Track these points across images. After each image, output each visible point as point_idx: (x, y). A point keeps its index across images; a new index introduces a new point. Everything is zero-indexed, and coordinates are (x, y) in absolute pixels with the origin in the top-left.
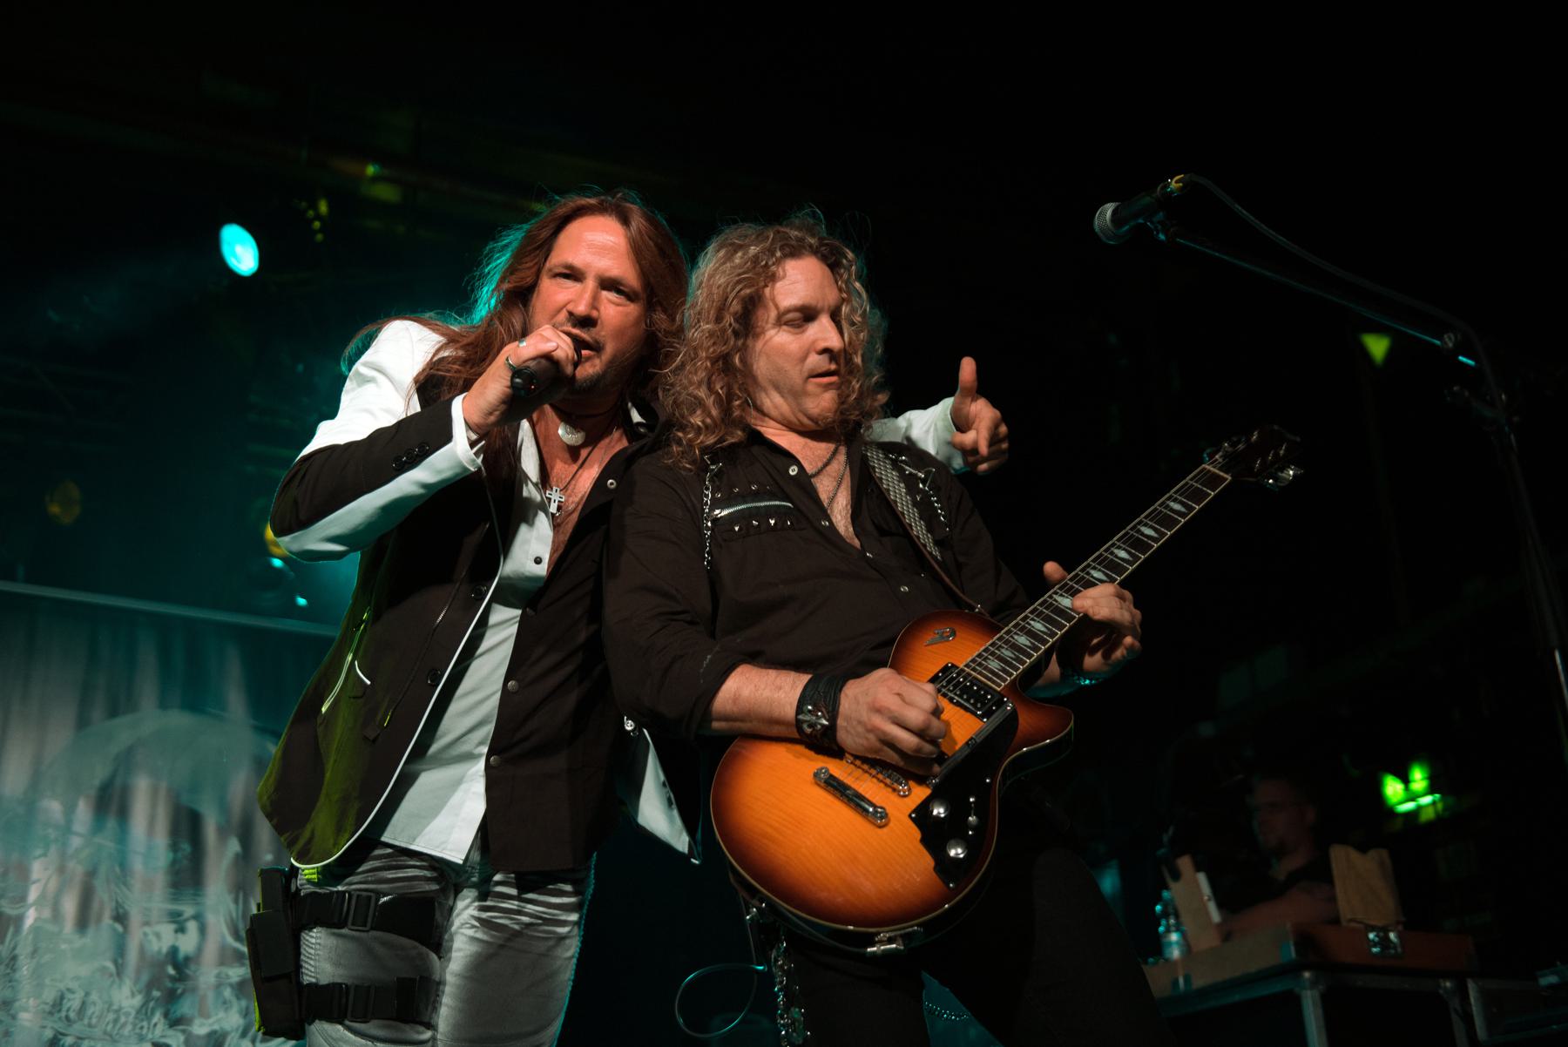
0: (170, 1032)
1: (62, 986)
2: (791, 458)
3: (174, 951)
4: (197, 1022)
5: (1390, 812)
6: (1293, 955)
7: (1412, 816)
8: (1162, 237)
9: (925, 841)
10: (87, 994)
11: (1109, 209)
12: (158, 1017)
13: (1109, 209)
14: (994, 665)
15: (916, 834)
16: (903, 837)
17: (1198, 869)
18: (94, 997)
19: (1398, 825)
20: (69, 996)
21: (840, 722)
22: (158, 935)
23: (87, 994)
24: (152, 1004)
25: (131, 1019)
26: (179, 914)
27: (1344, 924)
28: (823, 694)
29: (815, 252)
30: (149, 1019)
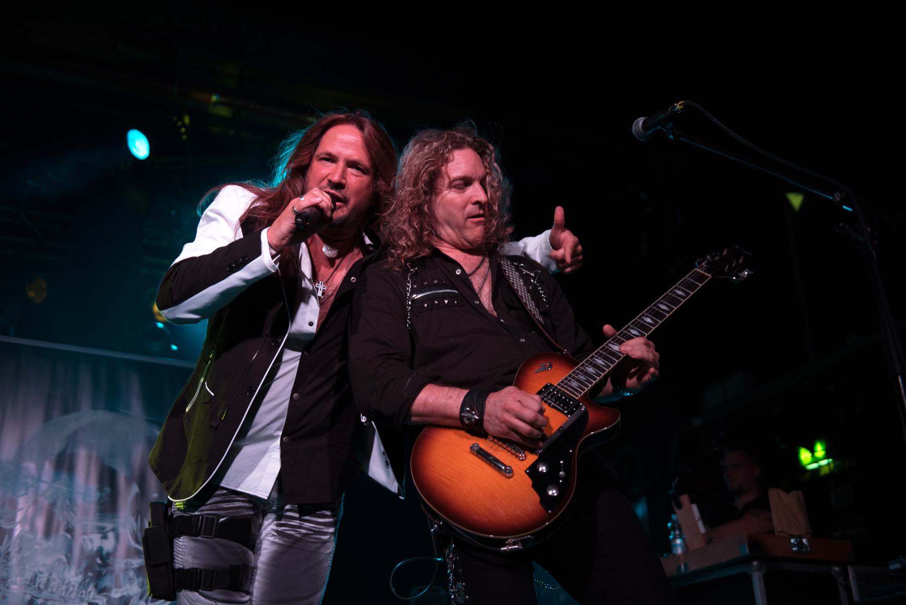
0: (98, 596)
1: (36, 570)
2: (457, 265)
3: (100, 549)
4: (114, 590)
6: (747, 551)
7: (816, 471)
9: (535, 486)
10: (50, 574)
11: (641, 121)
12: (91, 588)
13: (641, 121)
14: (574, 384)
15: (530, 482)
16: (521, 483)
18: (54, 576)
20: (40, 575)
21: (486, 417)
22: (91, 541)
23: (50, 574)
24: (88, 580)
25: (76, 589)
26: (104, 528)
27: (777, 534)
28: (476, 401)
29: (471, 146)
30: (86, 589)
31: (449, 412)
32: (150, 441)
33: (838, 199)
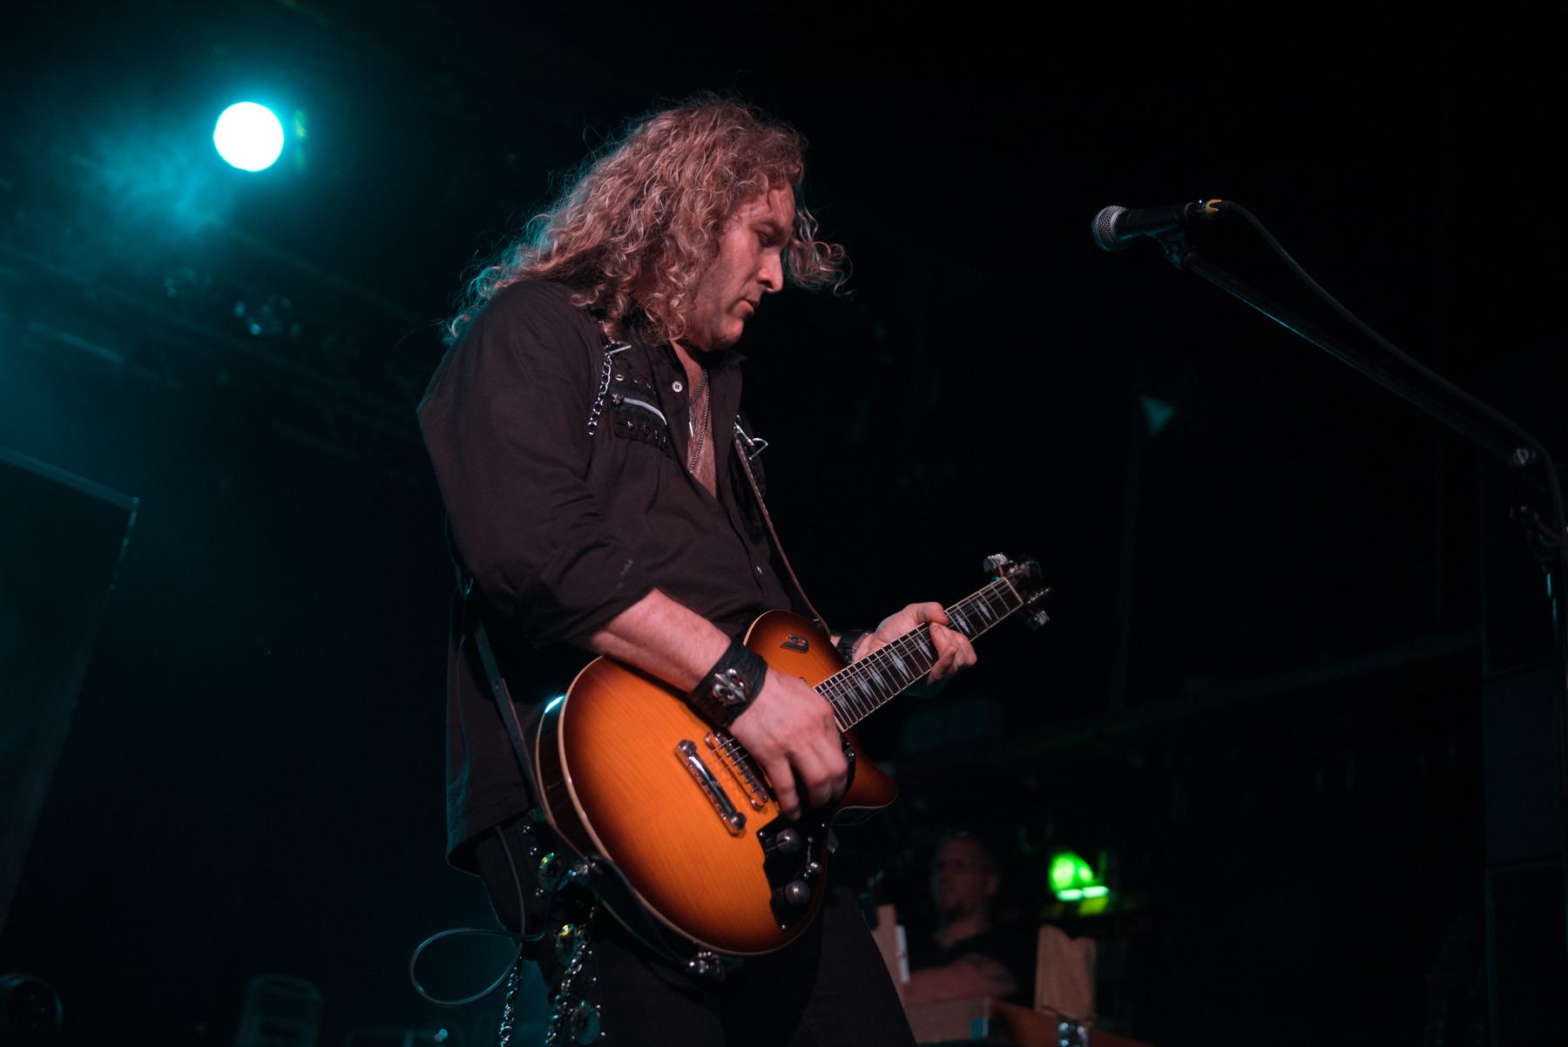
5: (1050, 896)
6: (985, 1032)
7: (1073, 905)
8: (1176, 259)
9: (769, 867)
11: (1114, 213)
13: (1114, 213)
16: (749, 855)
17: (899, 922)
19: (1057, 911)
27: (1038, 1008)
31: (678, 663)
32: (523, 250)
33: (1523, 461)
